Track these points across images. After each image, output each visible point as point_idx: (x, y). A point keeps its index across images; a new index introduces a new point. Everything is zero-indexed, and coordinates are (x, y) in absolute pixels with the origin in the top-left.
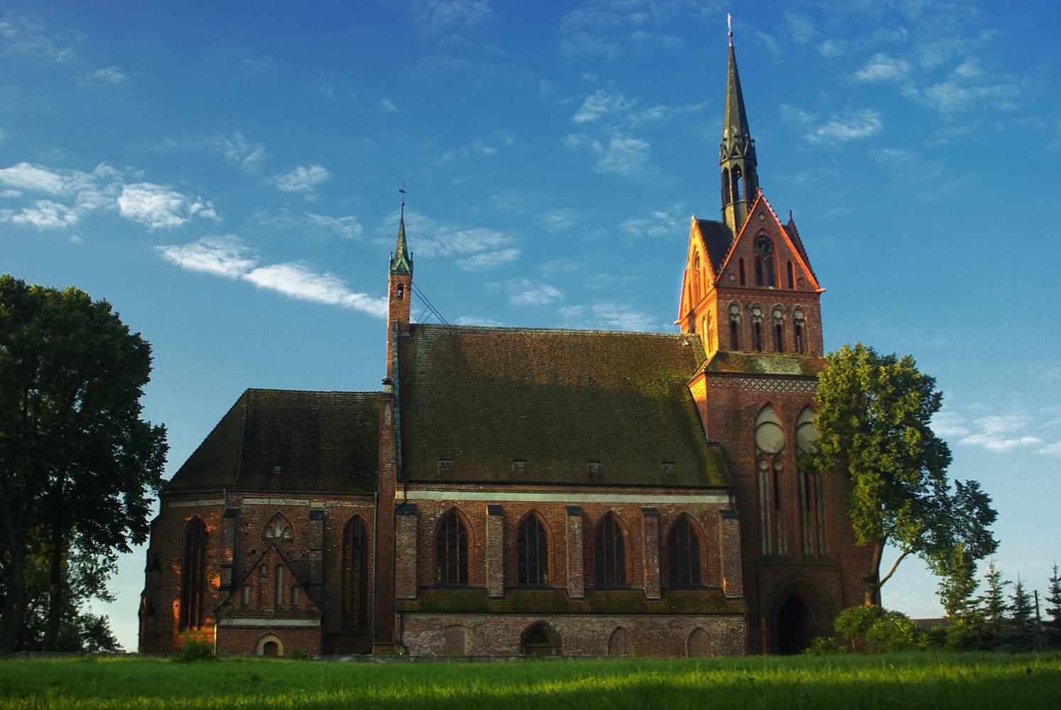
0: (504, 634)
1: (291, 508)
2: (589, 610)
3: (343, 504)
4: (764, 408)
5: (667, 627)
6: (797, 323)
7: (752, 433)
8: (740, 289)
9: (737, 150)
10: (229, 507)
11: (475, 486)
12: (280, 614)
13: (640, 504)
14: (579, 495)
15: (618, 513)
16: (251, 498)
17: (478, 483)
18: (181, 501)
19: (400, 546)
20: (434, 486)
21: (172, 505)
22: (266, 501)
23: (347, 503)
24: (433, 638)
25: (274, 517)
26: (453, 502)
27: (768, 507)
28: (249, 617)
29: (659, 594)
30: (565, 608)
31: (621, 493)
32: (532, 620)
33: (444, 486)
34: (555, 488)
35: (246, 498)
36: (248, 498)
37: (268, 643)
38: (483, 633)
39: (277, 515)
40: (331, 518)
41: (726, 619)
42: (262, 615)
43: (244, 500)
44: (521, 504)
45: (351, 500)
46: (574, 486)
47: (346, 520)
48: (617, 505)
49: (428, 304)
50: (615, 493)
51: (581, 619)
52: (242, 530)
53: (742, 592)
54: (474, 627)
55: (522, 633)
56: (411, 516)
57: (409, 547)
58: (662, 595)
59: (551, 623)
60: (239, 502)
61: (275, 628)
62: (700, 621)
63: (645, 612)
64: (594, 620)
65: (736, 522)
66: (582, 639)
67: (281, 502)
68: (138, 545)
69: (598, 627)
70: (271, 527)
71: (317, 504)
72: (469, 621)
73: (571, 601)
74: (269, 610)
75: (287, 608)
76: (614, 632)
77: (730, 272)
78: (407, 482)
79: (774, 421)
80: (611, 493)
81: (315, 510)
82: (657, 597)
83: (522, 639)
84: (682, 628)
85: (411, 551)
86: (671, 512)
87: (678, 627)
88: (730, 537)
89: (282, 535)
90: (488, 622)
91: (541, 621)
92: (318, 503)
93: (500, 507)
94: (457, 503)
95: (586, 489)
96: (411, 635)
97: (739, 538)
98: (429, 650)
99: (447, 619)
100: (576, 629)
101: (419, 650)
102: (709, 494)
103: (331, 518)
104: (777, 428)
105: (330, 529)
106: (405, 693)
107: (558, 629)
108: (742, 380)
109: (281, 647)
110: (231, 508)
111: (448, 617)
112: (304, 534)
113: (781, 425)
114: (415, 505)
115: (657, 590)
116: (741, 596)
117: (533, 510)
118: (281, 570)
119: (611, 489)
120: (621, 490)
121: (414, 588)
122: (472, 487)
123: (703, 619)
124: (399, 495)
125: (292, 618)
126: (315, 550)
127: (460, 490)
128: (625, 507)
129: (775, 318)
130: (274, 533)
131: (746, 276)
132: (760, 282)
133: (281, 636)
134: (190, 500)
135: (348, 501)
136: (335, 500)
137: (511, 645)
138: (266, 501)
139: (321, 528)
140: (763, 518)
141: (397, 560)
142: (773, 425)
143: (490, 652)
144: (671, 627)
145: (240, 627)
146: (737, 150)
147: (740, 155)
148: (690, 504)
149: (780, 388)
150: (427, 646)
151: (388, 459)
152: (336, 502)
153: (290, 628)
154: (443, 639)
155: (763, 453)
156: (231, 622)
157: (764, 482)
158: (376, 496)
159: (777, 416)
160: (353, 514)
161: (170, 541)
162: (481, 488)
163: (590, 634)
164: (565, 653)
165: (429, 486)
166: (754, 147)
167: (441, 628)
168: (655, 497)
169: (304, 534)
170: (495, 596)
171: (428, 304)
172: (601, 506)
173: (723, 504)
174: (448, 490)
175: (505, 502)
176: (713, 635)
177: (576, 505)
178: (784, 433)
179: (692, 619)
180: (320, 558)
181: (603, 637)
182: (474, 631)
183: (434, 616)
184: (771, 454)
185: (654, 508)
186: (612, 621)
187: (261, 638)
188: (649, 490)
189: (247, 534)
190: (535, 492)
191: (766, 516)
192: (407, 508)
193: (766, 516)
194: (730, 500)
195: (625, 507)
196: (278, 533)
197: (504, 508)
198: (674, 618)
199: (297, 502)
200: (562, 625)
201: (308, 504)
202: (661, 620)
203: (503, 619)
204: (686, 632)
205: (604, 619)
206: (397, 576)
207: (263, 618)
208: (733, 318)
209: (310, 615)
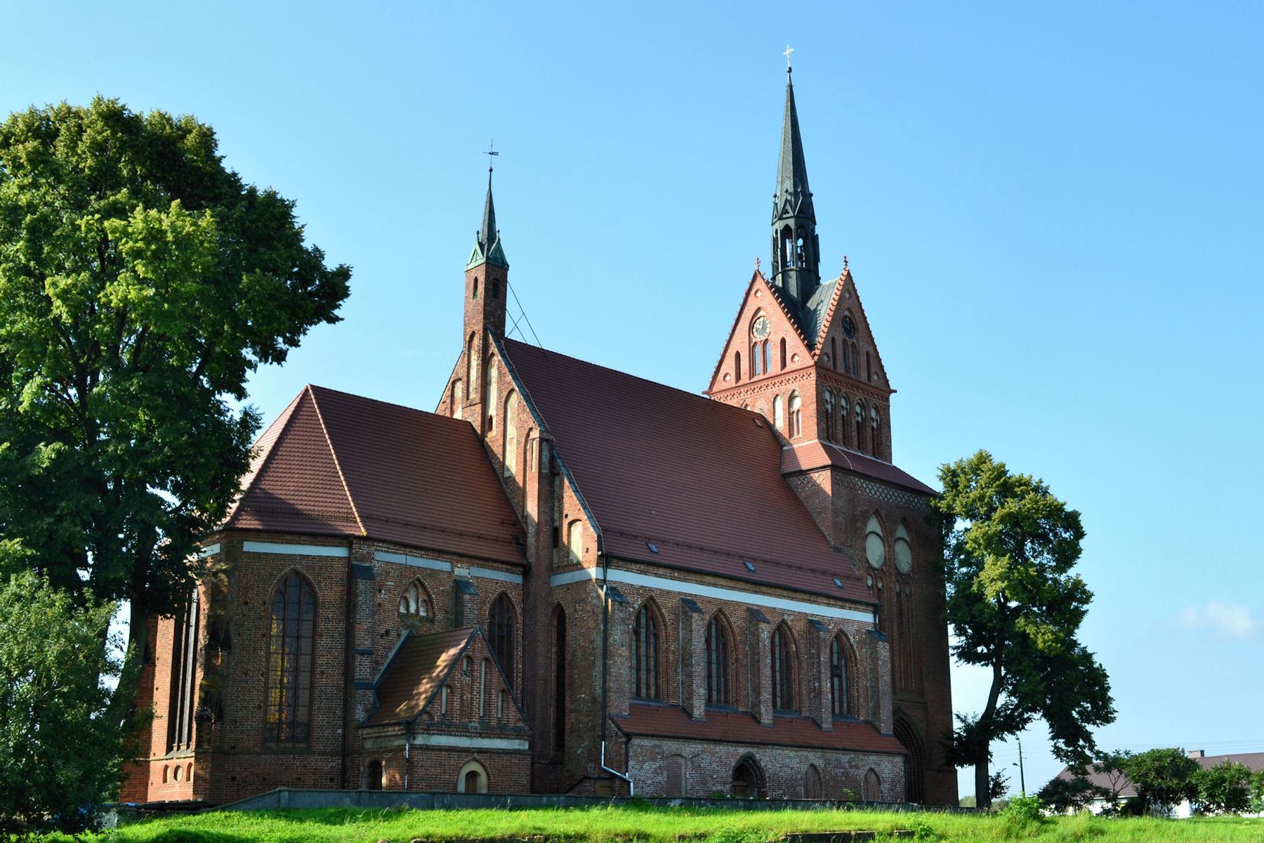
0: (719, 768)
1: (433, 574)
5: (847, 765)
9: (788, 207)
12: (486, 732)
15: (790, 623)
19: (613, 645)
20: (633, 566)
26: (650, 589)
32: (742, 751)
33: (642, 567)
38: (700, 767)
39: (418, 582)
41: (891, 758)
42: (465, 732)
47: (492, 597)
57: (623, 646)
59: (757, 756)
61: (481, 751)
69: (794, 764)
74: (473, 724)
80: (784, 597)
90: (703, 752)
91: (750, 752)
96: (636, 767)
106: (184, 819)
107: (763, 764)
110: (359, 563)
113: (881, 534)
119: (785, 593)
125: (499, 737)
127: (656, 575)
130: (408, 608)
133: (487, 764)
144: (851, 767)
145: (440, 749)
146: (788, 207)
147: (791, 214)
154: (665, 773)
156: (429, 739)
159: (879, 526)
161: (246, 603)
162: (676, 575)
163: (789, 772)
167: (662, 758)
178: (884, 546)
190: (723, 587)
198: (853, 756)
205: (800, 754)
209: (518, 735)
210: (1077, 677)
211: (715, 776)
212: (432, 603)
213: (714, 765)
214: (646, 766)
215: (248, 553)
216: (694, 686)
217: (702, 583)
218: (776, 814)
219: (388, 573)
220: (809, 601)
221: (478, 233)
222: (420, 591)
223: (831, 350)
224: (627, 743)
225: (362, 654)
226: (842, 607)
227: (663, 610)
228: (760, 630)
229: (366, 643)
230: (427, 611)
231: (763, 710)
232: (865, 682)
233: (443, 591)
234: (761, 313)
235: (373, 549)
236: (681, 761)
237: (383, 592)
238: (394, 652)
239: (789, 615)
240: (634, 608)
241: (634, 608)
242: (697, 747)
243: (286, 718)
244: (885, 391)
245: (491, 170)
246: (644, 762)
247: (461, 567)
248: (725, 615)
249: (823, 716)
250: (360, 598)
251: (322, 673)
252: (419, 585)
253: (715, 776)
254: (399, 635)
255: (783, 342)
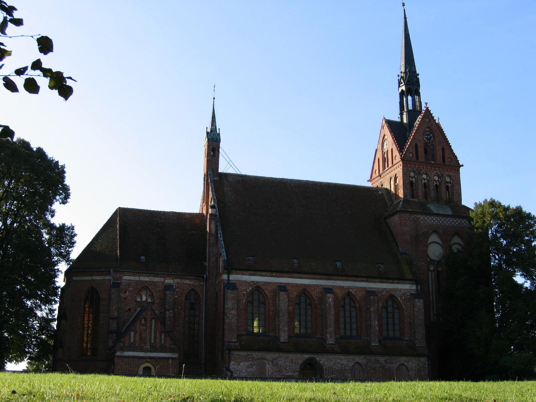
0: (290, 365)
1: (153, 283)
2: (339, 351)
3: (185, 281)
4: (432, 233)
5: (384, 362)
6: (447, 184)
7: (425, 248)
8: (415, 162)
10: (114, 281)
11: (270, 273)
12: (153, 349)
13: (366, 288)
14: (332, 281)
15: (354, 293)
16: (128, 275)
17: (272, 271)
18: (81, 276)
21: (74, 278)
22: (137, 278)
23: (187, 281)
24: (248, 366)
25: (142, 288)
26: (257, 282)
27: (434, 293)
28: (134, 351)
29: (378, 343)
30: (325, 350)
31: (355, 281)
32: (306, 356)
34: (317, 276)
35: (125, 275)
36: (127, 275)
37: (146, 367)
38: (278, 364)
39: (145, 287)
40: (177, 290)
42: (142, 350)
43: (124, 277)
44: (297, 285)
45: (189, 279)
46: (328, 275)
48: (353, 288)
49: (229, 161)
50: (352, 280)
51: (335, 356)
52: (123, 295)
53: (425, 343)
54: (272, 360)
55: (301, 364)
56: (234, 291)
57: (233, 309)
58: (380, 343)
59: (318, 359)
60: (120, 278)
61: (150, 358)
62: (403, 359)
63: (371, 353)
64: (342, 357)
65: (421, 301)
66: (335, 369)
67: (146, 279)
68: (478, 203)
70: (140, 294)
71: (168, 281)
72: (270, 356)
73: (328, 346)
74: (146, 346)
75: (158, 346)
76: (354, 365)
77: (410, 151)
78: (229, 269)
79: (437, 241)
80: (350, 280)
81: (167, 284)
82: (377, 345)
83: (301, 368)
84: (392, 364)
85: (234, 312)
86: (383, 293)
87: (390, 363)
88: (418, 310)
89: (147, 299)
91: (312, 357)
92: (169, 280)
93: (285, 287)
94: (259, 283)
95: (335, 277)
96: (235, 364)
97: (423, 311)
98: (246, 374)
99: (256, 355)
100: (332, 363)
101: (239, 374)
102: (405, 284)
103: (177, 290)
104: (439, 246)
105: (176, 297)
107: (321, 362)
108: (420, 216)
109: (153, 370)
110: (116, 281)
111: (257, 353)
112: (161, 299)
113: (442, 244)
114: (235, 284)
115: (377, 340)
116: (425, 346)
117: (304, 289)
118: (153, 321)
120: (356, 279)
121: (236, 335)
122: (269, 274)
123: (405, 358)
124: (225, 277)
125: (160, 352)
126: (169, 310)
127: (261, 275)
128: (357, 289)
129: (435, 180)
130: (141, 298)
131: (419, 154)
132: (426, 159)
134: (87, 276)
135: (187, 279)
136: (180, 279)
137: (294, 372)
138: (137, 278)
139: (172, 296)
140: (431, 299)
141: (225, 317)
142: (437, 244)
143: (282, 375)
144: (386, 363)
145: (128, 357)
148: (395, 289)
149: (441, 222)
150: (244, 371)
151: (213, 255)
152: (180, 280)
153: (159, 358)
155: (431, 260)
156: (123, 353)
157: (432, 278)
158: (205, 277)
159: (439, 239)
160: (190, 288)
162: (274, 274)
164: (326, 377)
165: (243, 272)
166: (419, 78)
168: (375, 284)
169: (161, 299)
170: (283, 341)
171: (229, 161)
172: (344, 288)
173: (413, 290)
174: (254, 275)
175: (288, 284)
176: (410, 368)
177: (329, 287)
178: (443, 248)
179: (398, 358)
180: (172, 315)
181: (348, 368)
182: (272, 362)
183: (249, 353)
184: (436, 261)
185: (374, 291)
186: (353, 358)
187: (142, 364)
188: (371, 280)
189: (125, 298)
190: (305, 278)
191: (433, 298)
192: (232, 286)
193: (433, 298)
194: (417, 287)
195: (357, 289)
196: (144, 298)
197: (287, 288)
198: (388, 358)
199: (157, 279)
200: (323, 360)
201: (163, 281)
202: (381, 358)
203: (290, 355)
204: (395, 366)
205: (348, 357)
206: (225, 327)
207: (142, 351)
208: (411, 179)
209: (172, 351)
210: (46, 313)
211: (288, 368)
212: (153, 296)
213: (287, 363)
214: (242, 364)
215: (75, 280)
216: (281, 326)
217: (292, 277)
218: (261, 382)
219: (130, 285)
220: (368, 281)
221: (207, 128)
222: (148, 291)
223: (414, 150)
224: (229, 353)
225: (113, 319)
226: (392, 283)
227: (266, 292)
228: (327, 298)
229: (115, 314)
230: (152, 299)
231: (328, 336)
232: (409, 320)
233: (159, 290)
234: (386, 137)
235: (122, 275)
236: (265, 361)
237: (127, 292)
238: (133, 318)
239: (353, 289)
240: (247, 292)
241: (247, 292)
242: (276, 355)
243: (90, 346)
244: (456, 166)
245: (214, 98)
246: (241, 362)
247: (169, 279)
248: (308, 292)
249: (372, 338)
250: (113, 296)
251: (102, 327)
252: (147, 289)
253: (288, 368)
254: (136, 310)
255: (392, 149)
